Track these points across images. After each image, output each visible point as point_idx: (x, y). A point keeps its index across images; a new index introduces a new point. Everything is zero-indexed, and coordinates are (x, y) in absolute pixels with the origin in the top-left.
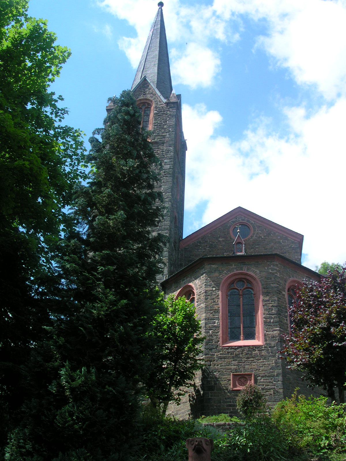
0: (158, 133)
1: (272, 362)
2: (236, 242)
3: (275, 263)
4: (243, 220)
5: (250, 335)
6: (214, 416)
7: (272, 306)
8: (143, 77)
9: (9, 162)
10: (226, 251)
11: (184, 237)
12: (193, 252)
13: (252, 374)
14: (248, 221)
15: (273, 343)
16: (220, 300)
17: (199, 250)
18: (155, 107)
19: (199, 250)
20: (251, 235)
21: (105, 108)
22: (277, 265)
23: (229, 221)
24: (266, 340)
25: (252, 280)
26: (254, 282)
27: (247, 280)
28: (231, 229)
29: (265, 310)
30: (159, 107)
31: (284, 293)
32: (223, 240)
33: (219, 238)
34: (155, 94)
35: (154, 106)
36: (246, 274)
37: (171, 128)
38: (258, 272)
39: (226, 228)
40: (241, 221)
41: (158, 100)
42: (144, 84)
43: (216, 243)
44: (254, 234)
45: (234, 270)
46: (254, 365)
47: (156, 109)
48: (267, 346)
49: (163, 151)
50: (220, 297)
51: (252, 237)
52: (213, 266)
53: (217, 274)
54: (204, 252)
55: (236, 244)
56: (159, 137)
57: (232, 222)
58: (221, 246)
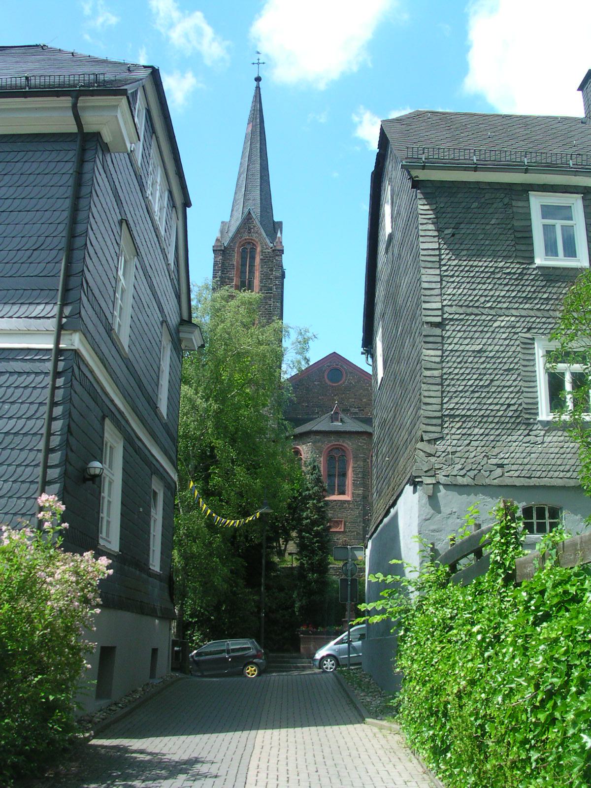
1: (357, 512)
3: (363, 438)
4: (337, 365)
5: (342, 493)
6: (379, 602)
7: (360, 472)
8: (246, 211)
13: (342, 521)
14: (341, 366)
15: (358, 499)
16: (322, 465)
20: (343, 379)
21: (211, 249)
22: (364, 439)
24: (353, 497)
25: (345, 449)
26: (347, 451)
27: (343, 450)
29: (354, 474)
30: (265, 252)
31: (368, 460)
35: (259, 249)
36: (342, 445)
38: (351, 444)
40: (335, 366)
42: (248, 219)
44: (346, 380)
45: (333, 441)
46: (344, 515)
48: (355, 501)
49: (270, 307)
50: (322, 462)
51: (344, 383)
52: (317, 437)
53: (320, 444)
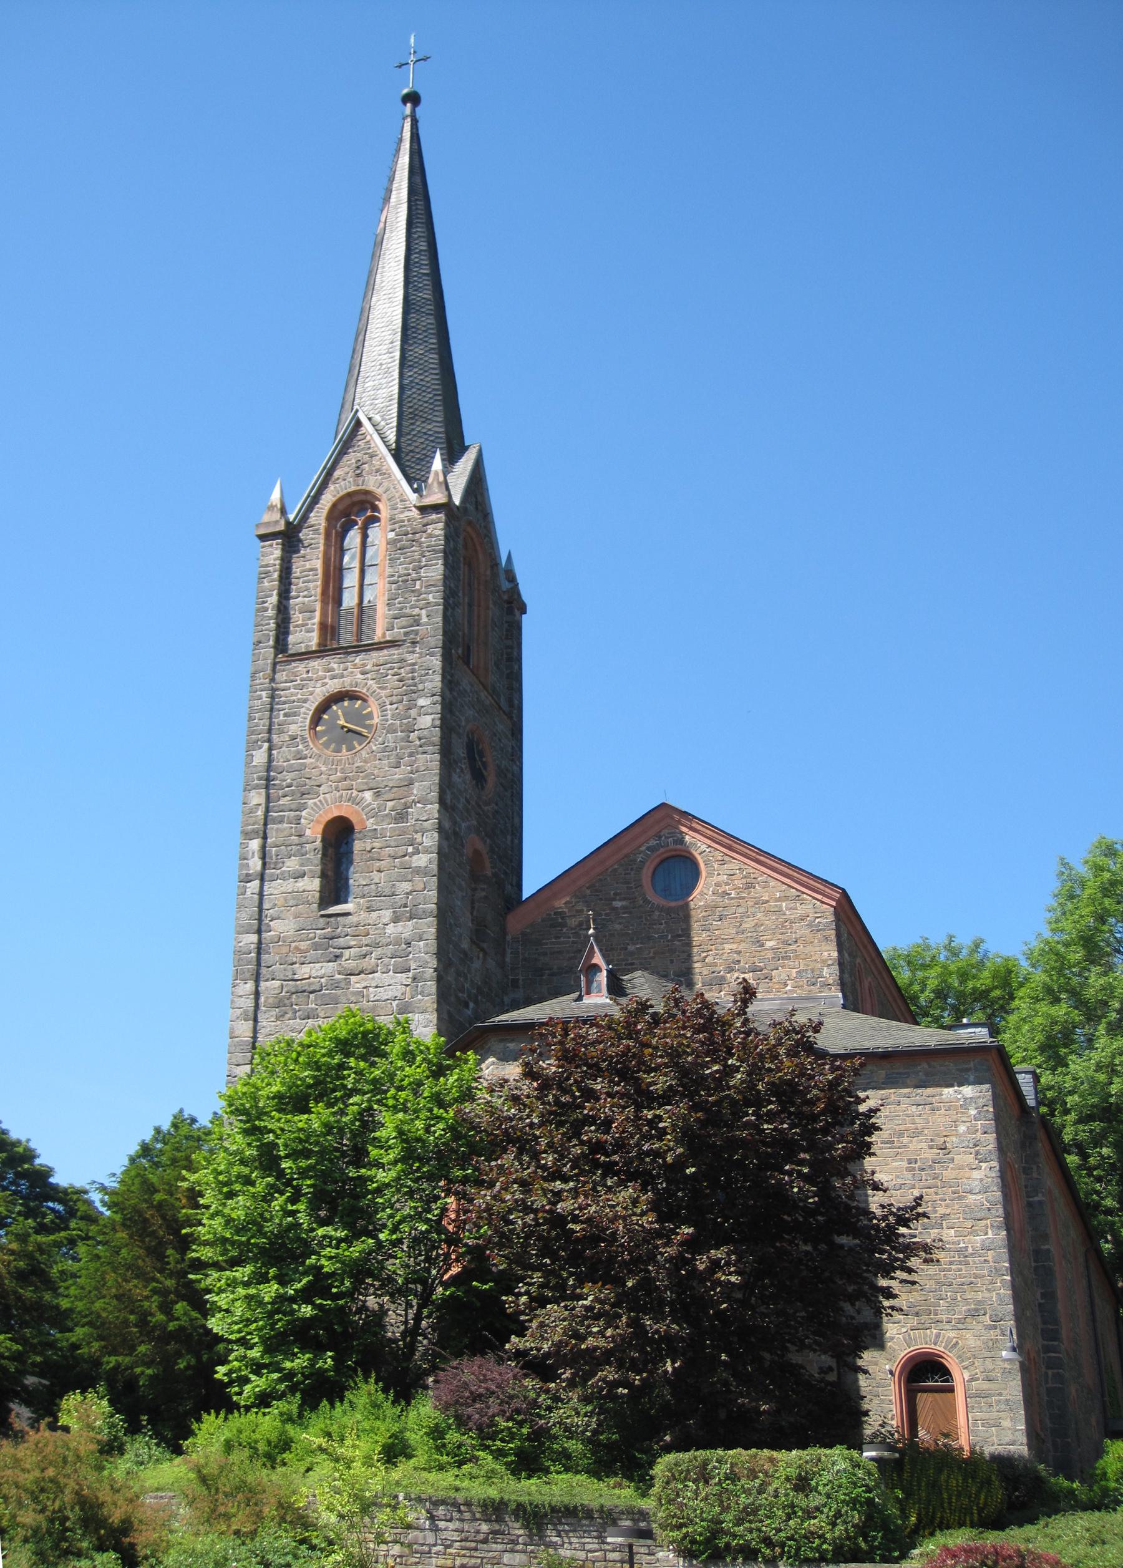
0: (401, 609)
2: (587, 965)
9: (7, 1173)
10: (632, 940)
11: (526, 894)
12: (547, 944)
17: (562, 939)
18: (392, 519)
19: (559, 938)
23: (640, 847)
28: (645, 871)
32: (623, 907)
33: (614, 899)
34: (387, 475)
37: (431, 592)
39: (632, 869)
41: (397, 495)
43: (606, 915)
47: (394, 524)
54: (573, 942)
55: (587, 971)
56: (403, 621)
57: (648, 849)
58: (620, 923)
